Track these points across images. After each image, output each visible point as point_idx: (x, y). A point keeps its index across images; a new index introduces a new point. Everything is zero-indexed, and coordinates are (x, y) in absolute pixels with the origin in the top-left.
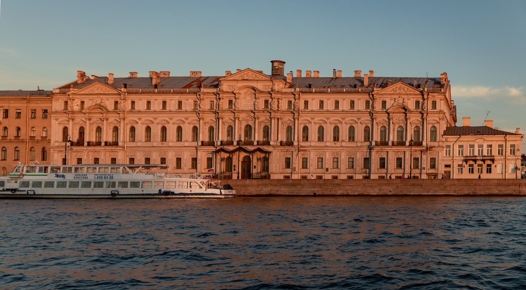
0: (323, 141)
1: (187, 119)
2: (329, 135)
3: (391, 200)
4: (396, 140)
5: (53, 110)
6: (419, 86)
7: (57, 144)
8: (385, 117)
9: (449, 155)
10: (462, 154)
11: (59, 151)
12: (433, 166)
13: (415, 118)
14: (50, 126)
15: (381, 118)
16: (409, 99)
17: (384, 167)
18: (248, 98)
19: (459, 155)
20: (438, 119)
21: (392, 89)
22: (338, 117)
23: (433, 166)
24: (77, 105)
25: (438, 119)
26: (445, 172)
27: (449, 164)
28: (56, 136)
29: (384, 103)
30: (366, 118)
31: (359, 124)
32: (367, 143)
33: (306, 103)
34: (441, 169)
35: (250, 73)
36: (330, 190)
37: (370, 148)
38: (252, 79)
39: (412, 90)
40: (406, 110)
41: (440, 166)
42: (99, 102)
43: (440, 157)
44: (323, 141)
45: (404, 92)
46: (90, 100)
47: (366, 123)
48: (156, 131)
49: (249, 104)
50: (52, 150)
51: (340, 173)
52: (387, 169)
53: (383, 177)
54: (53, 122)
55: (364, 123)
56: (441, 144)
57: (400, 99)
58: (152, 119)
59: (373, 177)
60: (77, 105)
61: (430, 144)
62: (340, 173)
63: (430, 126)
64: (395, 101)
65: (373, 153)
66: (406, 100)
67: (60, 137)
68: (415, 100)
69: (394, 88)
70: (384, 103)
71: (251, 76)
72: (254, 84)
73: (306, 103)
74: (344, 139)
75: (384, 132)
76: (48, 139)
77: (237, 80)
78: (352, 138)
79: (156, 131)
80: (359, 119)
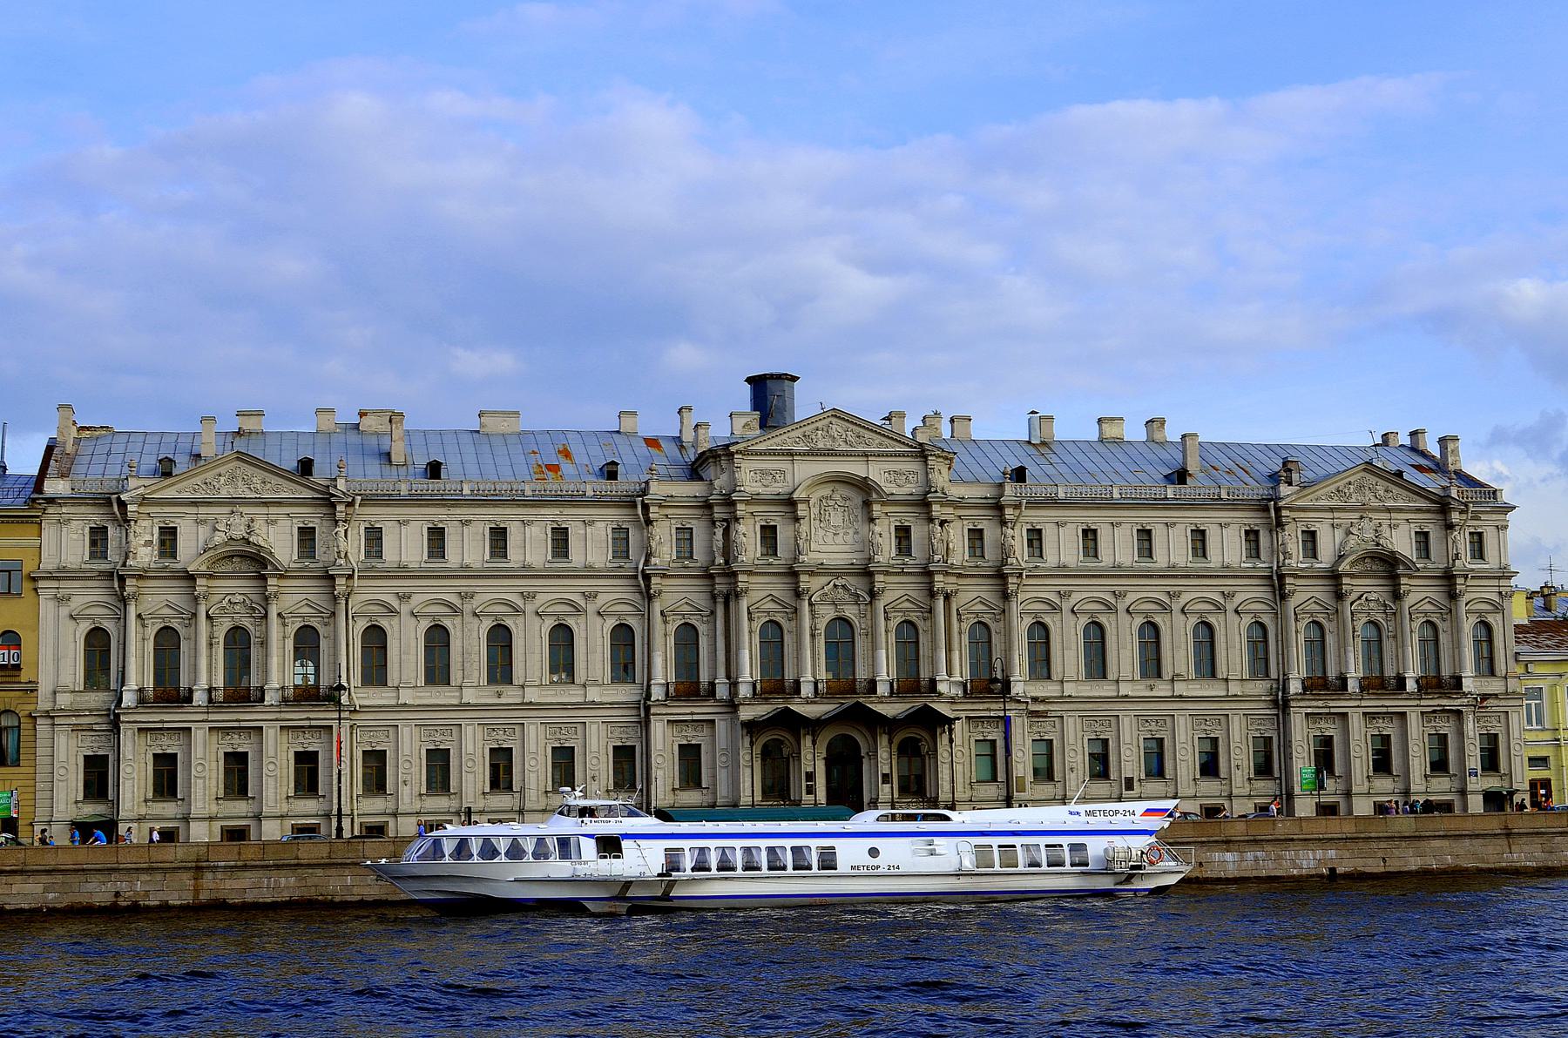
0: (447, 682)
1: (528, 597)
2: (1179, 652)
3: (273, 937)
4: (219, 682)
5: (48, 564)
6: (306, 467)
7: (64, 700)
8: (779, 588)
9: (1539, 722)
10: (1539, 722)
11: (76, 729)
12: (1491, 762)
13: (294, 600)
14: (36, 627)
15: (158, 601)
16: (274, 522)
17: (172, 792)
18: (836, 518)
19: (1530, 722)
20: (1495, 597)
21: (1333, 488)
22: (572, 591)
23: (1491, 762)
24: (149, 543)
25: (1495, 597)
26: (1534, 784)
27: (1543, 754)
28: (56, 661)
29: (168, 537)
30: (615, 596)
31: (1231, 615)
32: (97, 699)
33: (1035, 537)
34: (1523, 776)
35: (837, 427)
36: (1380, 854)
37: (1281, 704)
38: (844, 447)
39: (288, 491)
40: (263, 563)
41: (1516, 762)
42: (239, 532)
43: (1515, 733)
44: (447, 682)
45: (1375, 504)
46: (198, 522)
47: (619, 615)
48: (469, 644)
49: (839, 539)
50: (43, 726)
51: (395, 815)
52: (522, 791)
53: (312, 829)
54: (47, 607)
55: (1084, 612)
56: (1513, 685)
57: (1365, 524)
58: (1054, 598)
59: (200, 833)
60: (149, 543)
61: (1040, 689)
62: (395, 815)
63: (1473, 619)
64: (1348, 533)
65: (658, 729)
66: (259, 525)
67: (73, 669)
68: (1414, 528)
69: (1341, 484)
70: (168, 537)
71: (840, 435)
72: (857, 469)
73: (1035, 537)
74: (1181, 669)
75: (168, 644)
76: (24, 677)
77: (791, 454)
78: (1207, 665)
79: (469, 644)
80: (464, 596)
